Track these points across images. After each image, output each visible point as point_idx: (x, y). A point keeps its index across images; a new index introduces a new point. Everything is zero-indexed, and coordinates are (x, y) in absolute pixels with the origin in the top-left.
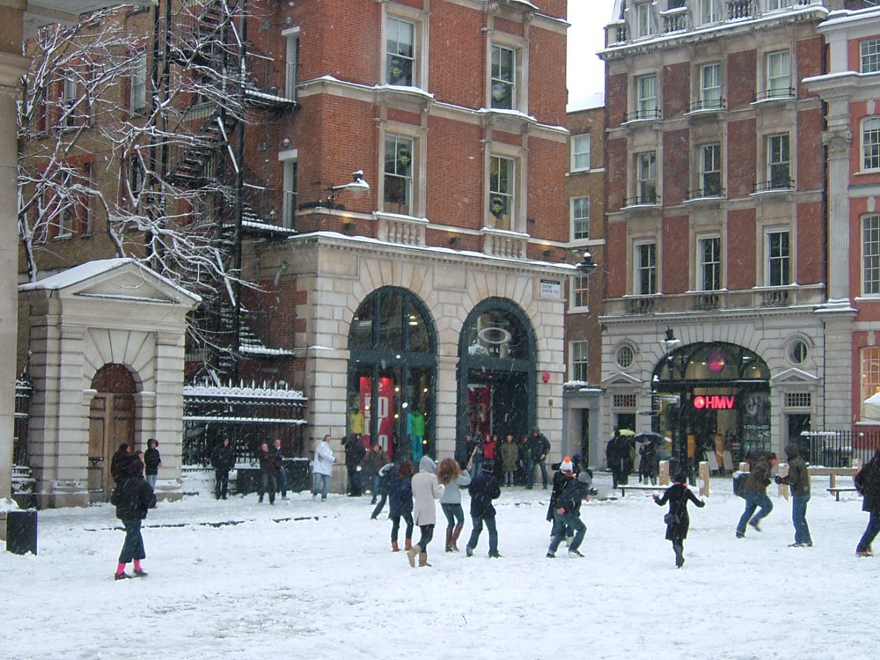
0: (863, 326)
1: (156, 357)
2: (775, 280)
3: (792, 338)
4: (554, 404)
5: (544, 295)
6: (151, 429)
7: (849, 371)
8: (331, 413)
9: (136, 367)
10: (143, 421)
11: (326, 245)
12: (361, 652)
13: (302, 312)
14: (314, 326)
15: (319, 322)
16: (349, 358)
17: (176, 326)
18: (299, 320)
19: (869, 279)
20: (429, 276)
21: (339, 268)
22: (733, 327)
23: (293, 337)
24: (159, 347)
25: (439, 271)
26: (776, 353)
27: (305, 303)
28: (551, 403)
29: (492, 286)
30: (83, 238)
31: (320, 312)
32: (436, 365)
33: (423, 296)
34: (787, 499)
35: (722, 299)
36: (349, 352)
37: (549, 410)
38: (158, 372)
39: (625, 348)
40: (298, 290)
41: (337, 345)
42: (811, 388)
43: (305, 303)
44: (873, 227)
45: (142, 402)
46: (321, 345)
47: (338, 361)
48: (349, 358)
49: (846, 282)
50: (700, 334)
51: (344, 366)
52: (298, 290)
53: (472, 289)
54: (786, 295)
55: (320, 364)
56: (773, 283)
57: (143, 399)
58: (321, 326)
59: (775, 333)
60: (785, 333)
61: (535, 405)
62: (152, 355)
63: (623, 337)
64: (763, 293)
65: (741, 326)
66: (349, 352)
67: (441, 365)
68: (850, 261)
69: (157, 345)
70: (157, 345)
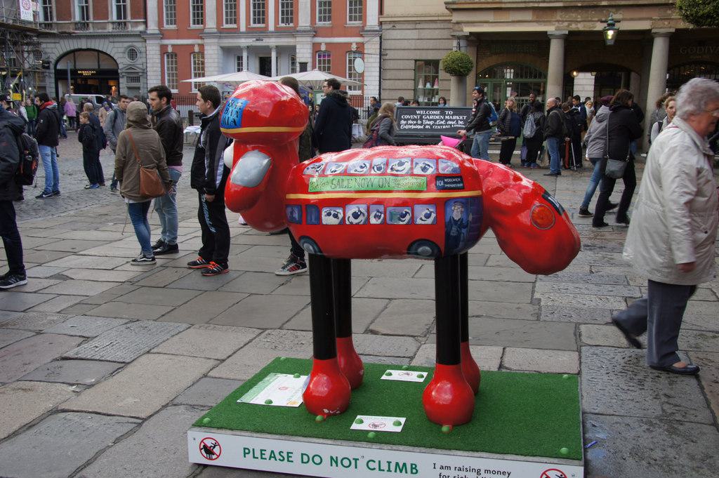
0: (166, 42)
2: (119, 17)
3: (127, 48)
7: (159, 65)
18: (130, 197)
19: (202, 13)
22: (97, 41)
26: (121, 55)
35: (91, 25)
39: (132, 50)
42: (140, 74)
44: (47, 7)
46: (495, 154)
47: (216, 469)
49: (157, 19)
50: (105, 47)
54: (88, 25)
56: (118, 19)
59: (121, 45)
60: (126, 45)
63: (131, 44)
64: (113, 23)
65: (102, 41)
68: (158, 5)
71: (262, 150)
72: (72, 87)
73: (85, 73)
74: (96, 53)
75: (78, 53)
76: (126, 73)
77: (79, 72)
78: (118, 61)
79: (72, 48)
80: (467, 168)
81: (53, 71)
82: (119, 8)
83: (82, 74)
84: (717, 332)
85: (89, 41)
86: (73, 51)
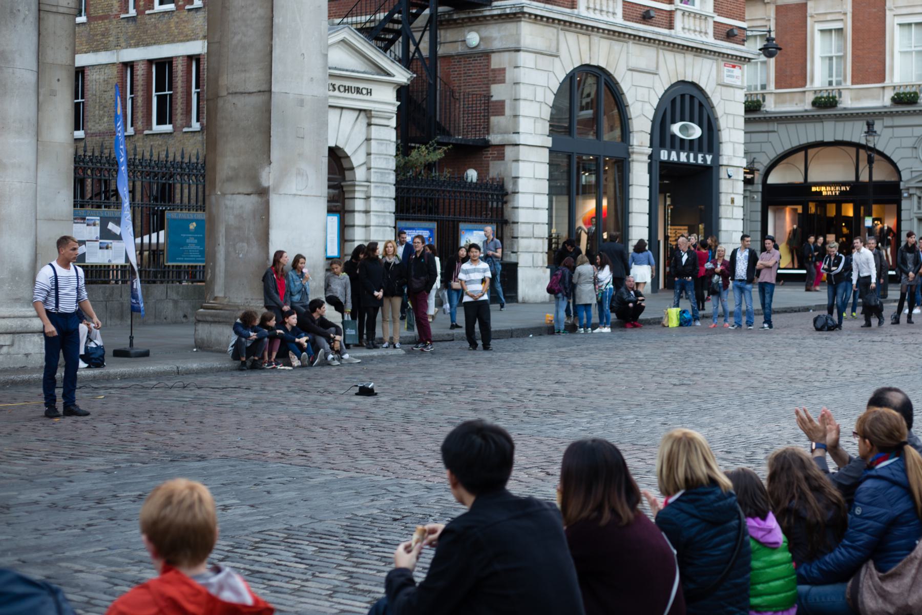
1: (368, 140)
4: (736, 203)
5: (727, 80)
6: (364, 224)
8: (534, 208)
9: (348, 151)
10: (356, 215)
11: (530, 14)
12: (254, 403)
13: (498, 92)
14: (515, 108)
15: (522, 103)
16: (550, 145)
17: (385, 100)
20: (624, 56)
21: (540, 45)
23: (488, 119)
24: (373, 127)
25: (633, 48)
27: (504, 82)
28: (733, 201)
29: (680, 69)
30: (189, 10)
31: (524, 92)
32: (629, 157)
33: (618, 77)
34: (84, 254)
36: (550, 139)
37: (730, 208)
38: (372, 156)
40: (493, 67)
41: (539, 131)
43: (504, 82)
45: (354, 191)
48: (550, 145)
51: (545, 155)
52: (493, 67)
53: (662, 72)
55: (523, 152)
57: (357, 188)
58: (525, 109)
61: (718, 204)
62: (364, 138)
66: (550, 139)
67: (634, 157)
69: (369, 125)
70: (369, 125)
71: (510, 495)
72: (122, 147)
73: (825, 191)
74: (853, 150)
75: (816, 150)
76: (917, 188)
77: (814, 189)
78: (900, 166)
79: (803, 141)
80: (77, 330)
81: (760, 188)
82: (161, 100)
83: (821, 192)
84: (40, 11)
85: (840, 125)
86: (805, 148)
